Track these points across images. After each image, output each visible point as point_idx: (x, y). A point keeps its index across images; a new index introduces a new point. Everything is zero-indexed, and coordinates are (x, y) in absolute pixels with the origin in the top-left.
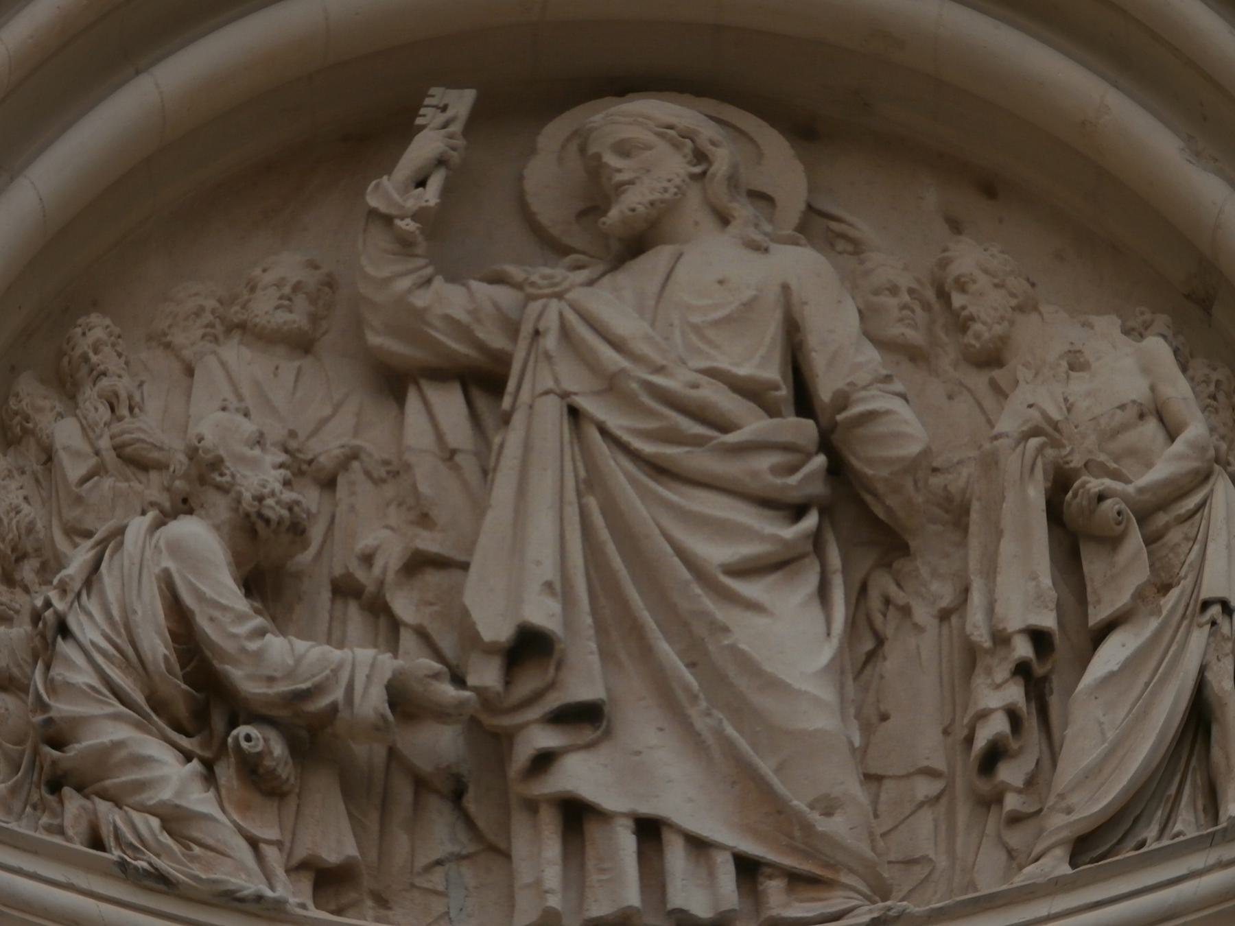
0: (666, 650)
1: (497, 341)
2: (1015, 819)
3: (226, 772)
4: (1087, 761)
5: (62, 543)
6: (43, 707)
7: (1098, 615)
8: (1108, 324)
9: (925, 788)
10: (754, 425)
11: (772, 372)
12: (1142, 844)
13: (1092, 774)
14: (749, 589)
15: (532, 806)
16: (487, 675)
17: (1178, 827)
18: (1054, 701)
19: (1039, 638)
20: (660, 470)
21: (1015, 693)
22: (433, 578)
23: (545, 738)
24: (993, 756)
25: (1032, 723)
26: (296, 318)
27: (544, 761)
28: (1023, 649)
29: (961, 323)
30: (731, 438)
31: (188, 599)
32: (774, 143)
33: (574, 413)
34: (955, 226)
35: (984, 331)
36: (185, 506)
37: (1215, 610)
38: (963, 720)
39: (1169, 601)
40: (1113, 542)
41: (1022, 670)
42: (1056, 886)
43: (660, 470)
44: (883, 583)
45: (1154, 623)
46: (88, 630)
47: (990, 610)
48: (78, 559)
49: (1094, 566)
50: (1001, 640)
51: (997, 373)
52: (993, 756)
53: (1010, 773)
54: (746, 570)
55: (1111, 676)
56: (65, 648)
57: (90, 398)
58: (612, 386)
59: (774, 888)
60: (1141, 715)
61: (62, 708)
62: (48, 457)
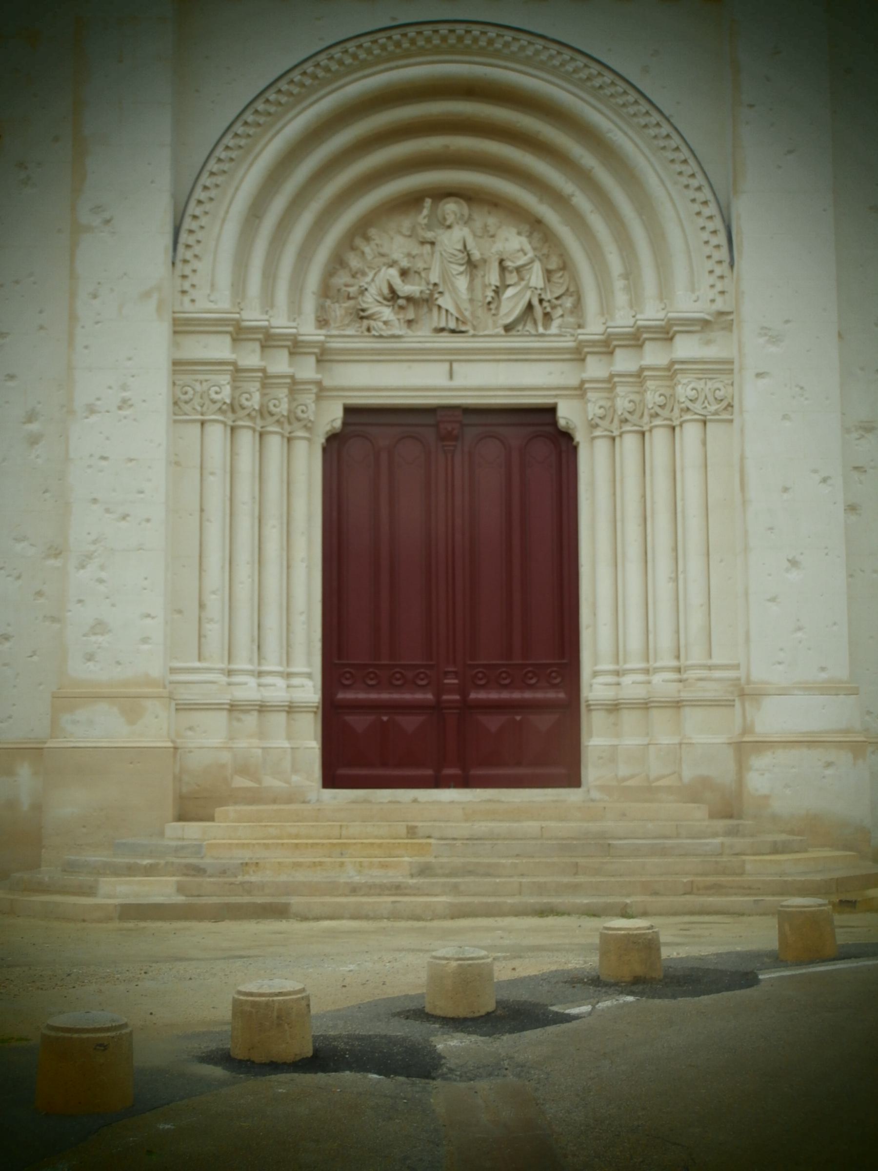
0: (193, 322)
1: (433, 240)
2: (494, 315)
3: (396, 306)
4: (507, 310)
5: (367, 270)
6: (361, 305)
7: (508, 283)
8: (514, 231)
9: (480, 304)
10: (461, 255)
11: (460, 246)
12: (518, 331)
13: (507, 315)
14: (457, 277)
15: (436, 305)
16: (431, 287)
17: (527, 328)
18: (500, 295)
19: (497, 287)
20: (450, 262)
21: (492, 294)
22: (426, 271)
23: (436, 296)
24: (489, 303)
25: (496, 298)
26: (408, 233)
27: (437, 299)
28: (494, 288)
29: (488, 231)
30: (457, 258)
31: (392, 283)
32: (464, 204)
33: (441, 254)
34: (489, 213)
35: (491, 233)
36: (391, 266)
37: (532, 289)
38: (467, 946)
39: (523, 283)
40: (511, 272)
41: (494, 291)
42: (501, 336)
43: (450, 262)
44: (474, 271)
45: (518, 288)
46: (373, 290)
47: (489, 279)
48: (371, 275)
49: (507, 275)
50: (490, 285)
51: (493, 239)
53: (493, 306)
54: (458, 274)
55: (508, 298)
56: (366, 293)
57: (373, 243)
58: (445, 251)
59: (460, 323)
60: (517, 304)
61: (364, 306)
62: (363, 253)
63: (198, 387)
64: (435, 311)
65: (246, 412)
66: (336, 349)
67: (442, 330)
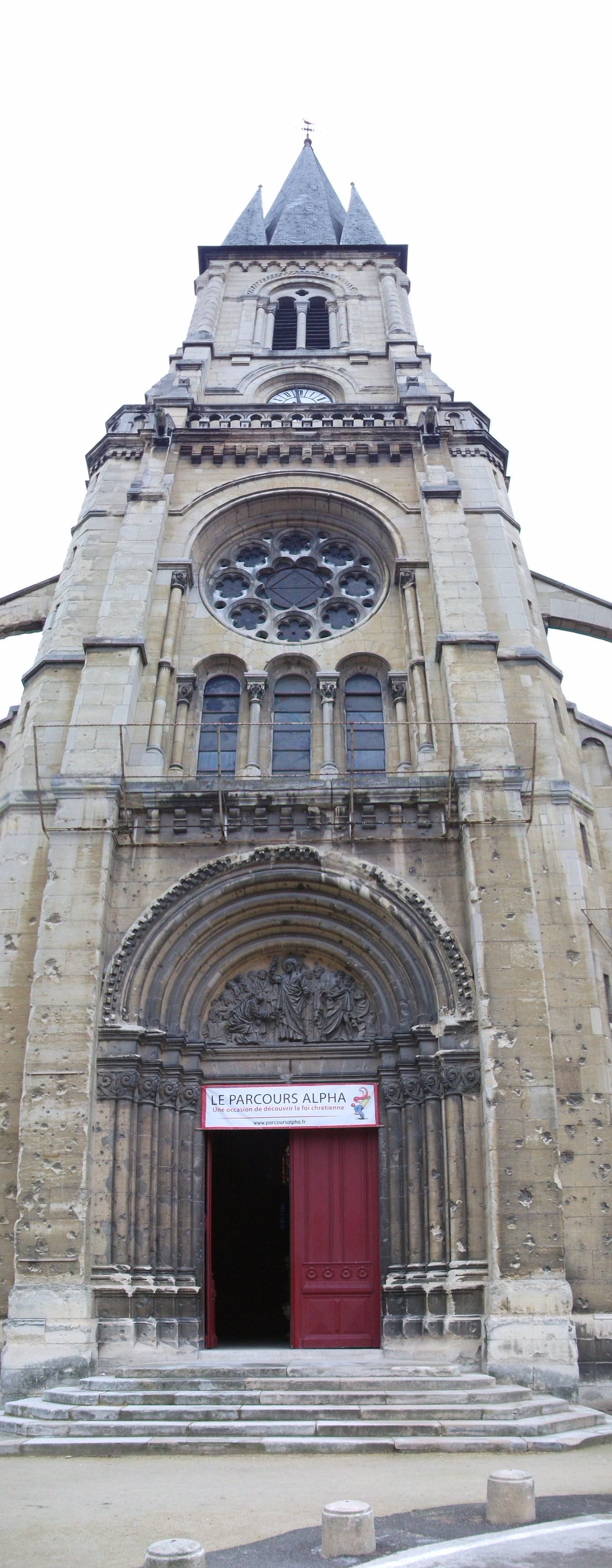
24: (317, 1021)
52: (317, 1021)
63: (114, 1077)
64: (281, 1026)
65: (148, 1093)
66: (133, 783)
67: (284, 1039)
